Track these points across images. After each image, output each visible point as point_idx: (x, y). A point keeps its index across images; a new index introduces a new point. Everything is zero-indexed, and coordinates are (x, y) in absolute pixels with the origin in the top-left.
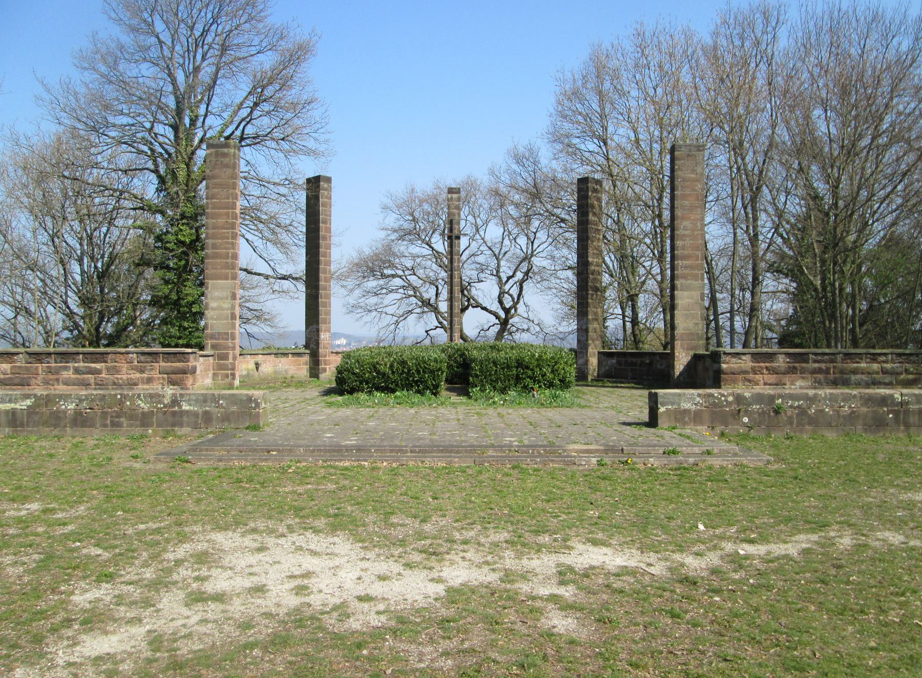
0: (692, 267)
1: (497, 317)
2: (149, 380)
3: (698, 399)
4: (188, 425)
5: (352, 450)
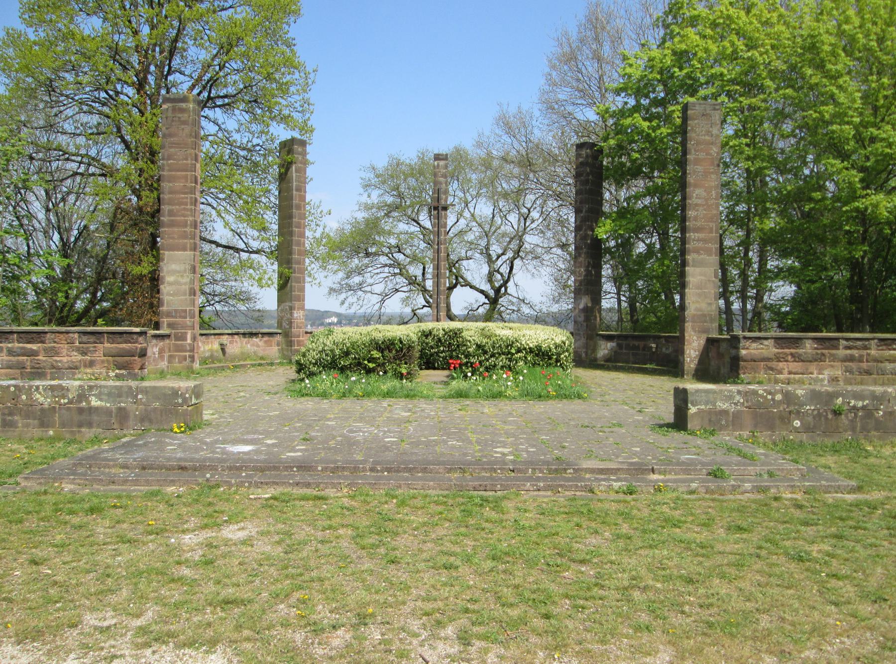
0: (705, 241)
1: (487, 296)
2: (91, 364)
3: (738, 398)
4: (98, 426)
5: (292, 467)
